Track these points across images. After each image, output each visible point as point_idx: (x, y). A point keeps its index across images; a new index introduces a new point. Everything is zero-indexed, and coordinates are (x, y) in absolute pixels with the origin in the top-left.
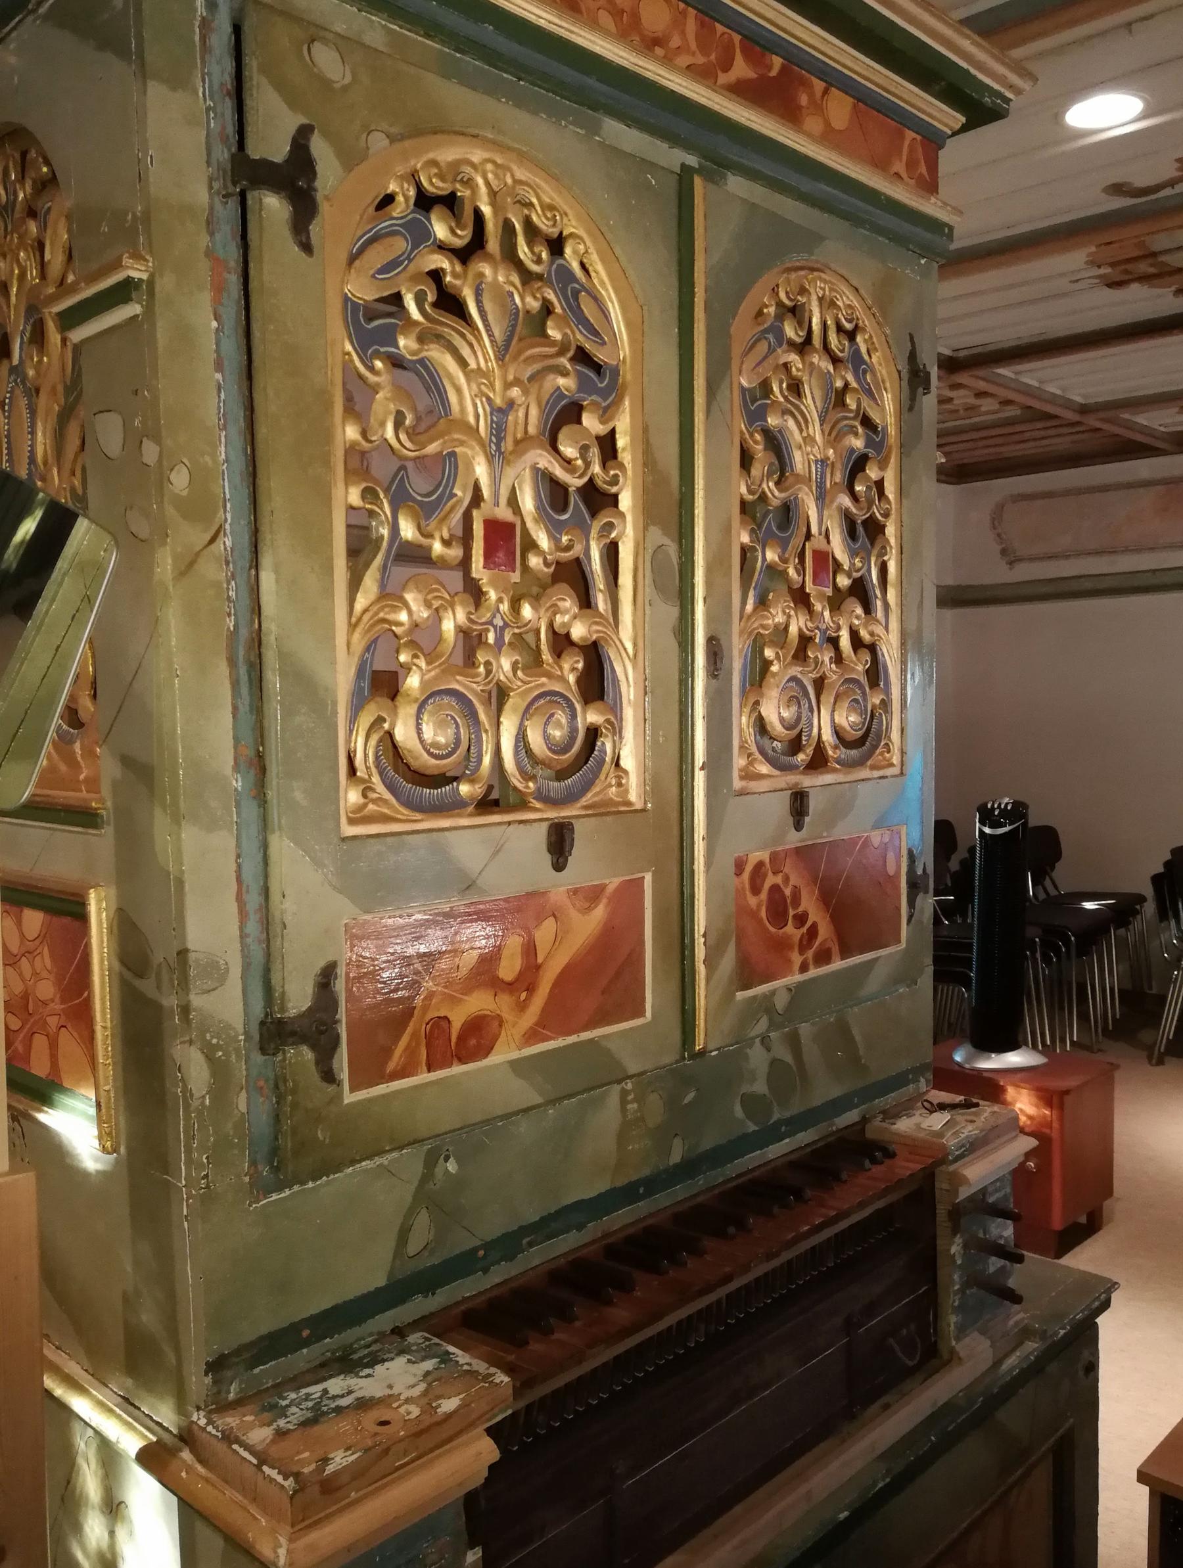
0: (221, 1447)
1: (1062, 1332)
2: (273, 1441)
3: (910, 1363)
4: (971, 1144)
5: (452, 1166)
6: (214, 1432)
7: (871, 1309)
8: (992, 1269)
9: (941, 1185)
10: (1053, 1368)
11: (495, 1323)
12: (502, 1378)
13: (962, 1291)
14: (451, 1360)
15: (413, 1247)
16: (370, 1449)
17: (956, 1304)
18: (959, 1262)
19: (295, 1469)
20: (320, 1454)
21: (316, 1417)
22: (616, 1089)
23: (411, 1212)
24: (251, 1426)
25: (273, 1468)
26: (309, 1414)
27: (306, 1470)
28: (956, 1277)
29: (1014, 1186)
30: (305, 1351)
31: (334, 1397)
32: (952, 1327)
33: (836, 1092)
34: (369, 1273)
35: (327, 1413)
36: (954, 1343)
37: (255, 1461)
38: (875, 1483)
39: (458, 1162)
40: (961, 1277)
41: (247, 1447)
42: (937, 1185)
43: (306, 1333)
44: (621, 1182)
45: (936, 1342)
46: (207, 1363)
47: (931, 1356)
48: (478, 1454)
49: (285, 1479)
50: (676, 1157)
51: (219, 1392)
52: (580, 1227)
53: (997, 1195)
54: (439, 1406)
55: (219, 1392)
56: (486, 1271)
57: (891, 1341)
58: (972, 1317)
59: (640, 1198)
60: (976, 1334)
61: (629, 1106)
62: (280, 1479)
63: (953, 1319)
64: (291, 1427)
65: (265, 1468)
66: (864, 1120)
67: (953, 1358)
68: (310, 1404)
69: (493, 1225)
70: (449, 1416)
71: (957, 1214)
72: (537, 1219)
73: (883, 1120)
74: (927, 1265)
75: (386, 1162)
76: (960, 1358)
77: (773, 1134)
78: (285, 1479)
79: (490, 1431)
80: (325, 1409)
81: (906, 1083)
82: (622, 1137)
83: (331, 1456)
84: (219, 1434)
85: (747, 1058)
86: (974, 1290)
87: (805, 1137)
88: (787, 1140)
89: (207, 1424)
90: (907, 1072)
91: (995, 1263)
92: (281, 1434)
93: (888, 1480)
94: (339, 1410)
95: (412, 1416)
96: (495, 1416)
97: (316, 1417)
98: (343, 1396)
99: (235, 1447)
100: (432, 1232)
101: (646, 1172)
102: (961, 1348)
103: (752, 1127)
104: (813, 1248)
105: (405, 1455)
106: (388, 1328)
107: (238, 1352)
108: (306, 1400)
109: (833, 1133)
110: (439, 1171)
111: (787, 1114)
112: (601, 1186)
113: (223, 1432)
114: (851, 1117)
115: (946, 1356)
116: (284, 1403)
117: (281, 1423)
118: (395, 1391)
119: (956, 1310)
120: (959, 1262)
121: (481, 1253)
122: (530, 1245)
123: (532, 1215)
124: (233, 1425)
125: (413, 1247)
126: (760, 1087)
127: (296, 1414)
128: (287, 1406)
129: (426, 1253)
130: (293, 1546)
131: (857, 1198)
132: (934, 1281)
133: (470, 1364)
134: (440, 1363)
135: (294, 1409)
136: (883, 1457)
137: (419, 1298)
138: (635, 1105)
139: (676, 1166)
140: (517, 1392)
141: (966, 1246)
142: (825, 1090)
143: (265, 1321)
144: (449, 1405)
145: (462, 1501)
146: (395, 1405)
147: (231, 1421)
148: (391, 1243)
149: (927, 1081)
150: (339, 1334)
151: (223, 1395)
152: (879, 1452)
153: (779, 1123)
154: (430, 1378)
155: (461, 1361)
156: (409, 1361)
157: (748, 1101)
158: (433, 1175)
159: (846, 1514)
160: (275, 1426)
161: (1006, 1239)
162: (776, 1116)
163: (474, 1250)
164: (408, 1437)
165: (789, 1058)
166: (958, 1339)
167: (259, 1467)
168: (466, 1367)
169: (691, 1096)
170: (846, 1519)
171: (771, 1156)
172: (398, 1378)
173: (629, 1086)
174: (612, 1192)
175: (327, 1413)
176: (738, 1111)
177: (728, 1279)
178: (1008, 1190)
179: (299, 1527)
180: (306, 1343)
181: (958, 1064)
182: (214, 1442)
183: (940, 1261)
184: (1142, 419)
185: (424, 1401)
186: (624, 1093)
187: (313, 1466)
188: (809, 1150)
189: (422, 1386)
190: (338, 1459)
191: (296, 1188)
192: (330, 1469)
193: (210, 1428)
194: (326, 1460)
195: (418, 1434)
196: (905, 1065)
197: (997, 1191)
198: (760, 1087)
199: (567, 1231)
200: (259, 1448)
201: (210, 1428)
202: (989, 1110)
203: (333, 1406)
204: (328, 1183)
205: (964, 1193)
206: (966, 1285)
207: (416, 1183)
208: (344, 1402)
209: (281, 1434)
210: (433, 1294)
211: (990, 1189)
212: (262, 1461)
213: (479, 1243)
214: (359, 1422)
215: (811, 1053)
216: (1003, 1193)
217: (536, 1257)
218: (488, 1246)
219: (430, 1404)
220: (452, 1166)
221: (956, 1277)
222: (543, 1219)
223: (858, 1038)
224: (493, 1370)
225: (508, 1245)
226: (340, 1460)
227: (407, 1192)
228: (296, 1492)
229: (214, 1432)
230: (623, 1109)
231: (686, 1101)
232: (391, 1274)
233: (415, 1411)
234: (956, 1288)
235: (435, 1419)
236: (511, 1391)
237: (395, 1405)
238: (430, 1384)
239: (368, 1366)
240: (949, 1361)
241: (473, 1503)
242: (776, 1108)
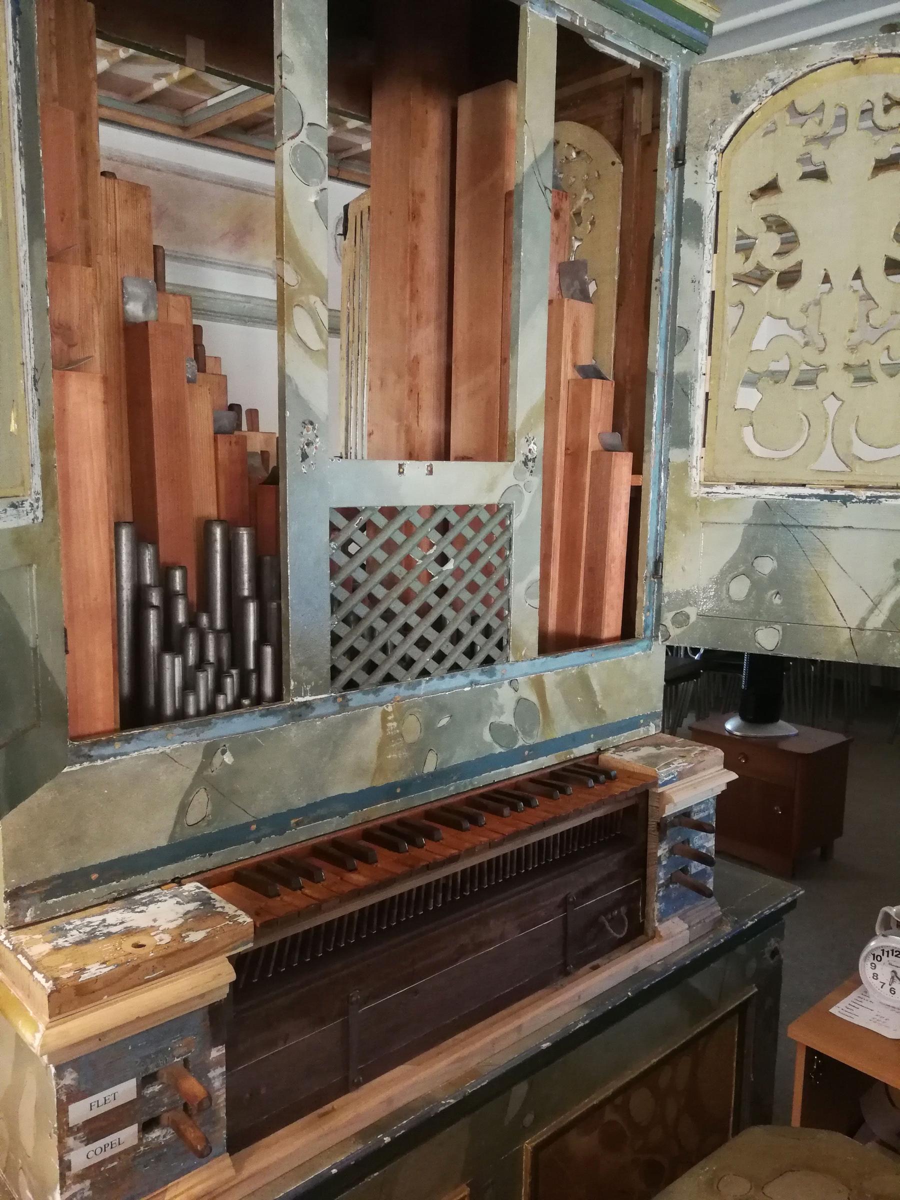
0: (10, 956)
1: (750, 923)
2: (48, 954)
3: (618, 936)
4: (679, 773)
5: (228, 759)
6: (8, 945)
7: (587, 893)
8: (693, 871)
9: (652, 802)
10: (741, 949)
11: (256, 881)
12: (245, 919)
13: (666, 885)
14: (210, 904)
15: (193, 817)
16: (122, 964)
17: (661, 894)
18: (664, 863)
19: (56, 975)
20: (80, 965)
21: (90, 938)
22: (379, 709)
23: (190, 792)
24: (36, 942)
25: (41, 973)
26: (84, 937)
27: (64, 977)
28: (661, 874)
29: (717, 811)
30: (94, 890)
31: (109, 925)
32: (656, 913)
33: (574, 728)
34: (154, 833)
35: (99, 936)
36: (657, 924)
37: (30, 968)
38: (576, 1023)
39: (234, 755)
40: (665, 874)
41: (27, 958)
42: (650, 803)
43: (94, 877)
44: (380, 782)
45: (643, 922)
46: (5, 892)
47: (638, 931)
48: (215, 977)
49: (47, 982)
50: (430, 766)
51: (16, 915)
52: (343, 815)
53: (702, 815)
54: (188, 936)
55: (16, 915)
56: (258, 841)
57: (603, 918)
58: (673, 907)
59: (397, 796)
60: (677, 919)
61: (389, 725)
62: (43, 981)
63: (657, 906)
64: (67, 944)
65: (35, 973)
66: (599, 751)
67: (655, 936)
68: (88, 929)
69: (265, 804)
70: (194, 945)
71: (663, 826)
72: (305, 805)
73: (614, 752)
74: (639, 863)
75: (168, 751)
76: (661, 937)
77: (518, 756)
78: (47, 982)
79: (230, 959)
80: (98, 933)
81: (638, 726)
82: (382, 749)
83: (87, 967)
84: (11, 947)
85: (496, 695)
86: (678, 885)
87: (547, 761)
88: (530, 762)
89: (5, 939)
90: (639, 717)
91: (696, 867)
92: (57, 949)
93: (587, 1022)
94: (109, 934)
95: (163, 943)
96: (238, 947)
97: (90, 938)
98: (116, 925)
99: (20, 956)
100: (210, 808)
101: (402, 776)
102: (663, 928)
103: (498, 750)
104: (540, 842)
105: (154, 972)
106: (169, 878)
107: (30, 887)
108: (87, 926)
109: (571, 760)
110: (216, 761)
111: (531, 742)
112: (363, 784)
113: (14, 945)
114: (588, 749)
115: (650, 933)
116: (68, 927)
117: (61, 942)
118: (157, 924)
119: (659, 899)
120: (664, 863)
121: (254, 827)
122: (298, 824)
123: (299, 801)
124: (24, 940)
125: (193, 817)
126: (507, 719)
127: (75, 936)
128: (70, 930)
129: (204, 824)
130: (48, 1032)
131: (581, 811)
132: (644, 877)
133: (223, 907)
134: (201, 905)
135: (75, 932)
136: (586, 1004)
137: (197, 858)
138: (395, 724)
139: (431, 774)
140: (259, 931)
141: (671, 851)
142: (565, 724)
143: (59, 864)
144: (196, 936)
145: (206, 1010)
146: (152, 934)
147: (22, 937)
148: (172, 812)
149: (657, 726)
150: (123, 878)
151: (20, 918)
152: (582, 1002)
153: (523, 748)
154: (188, 916)
155: (218, 904)
156: (178, 903)
157: (495, 729)
158: (211, 763)
159: (548, 1044)
160: (54, 943)
161: (708, 849)
162: (520, 743)
163: (248, 824)
164: (157, 958)
165: (533, 698)
166: (660, 921)
167: (31, 972)
168: (220, 910)
169: (444, 721)
170: (548, 1048)
171: (515, 774)
172: (163, 914)
173: (390, 709)
174: (372, 789)
175: (99, 936)
176: (487, 737)
177: (453, 859)
178: (712, 811)
179: (55, 1018)
180: (96, 884)
181: (730, 732)
182: (7, 953)
183: (650, 861)
184: (592, 41)
185: (178, 931)
186: (385, 715)
187: (71, 974)
188: (549, 770)
189: (181, 921)
190: (93, 970)
191: (86, 764)
192: (85, 977)
193: (6, 943)
194: (82, 970)
195: (165, 957)
196: (638, 711)
197: (701, 811)
198: (507, 719)
199: (331, 815)
200: (35, 958)
201: (6, 943)
202: (700, 749)
203: (105, 931)
204: (114, 763)
205: (670, 810)
206: (670, 881)
207: (195, 770)
208: (113, 930)
209: (57, 949)
210: (210, 855)
211: (695, 810)
212: (35, 968)
213: (252, 819)
214: (120, 944)
215: (554, 697)
216: (706, 813)
217: (301, 835)
218: (260, 822)
219: (180, 935)
220: (228, 759)
221: (661, 874)
222: (308, 805)
223: (596, 687)
224: (239, 912)
225: (278, 823)
226: (94, 970)
227: (187, 777)
228: (52, 992)
229: (8, 945)
230: (384, 727)
231: (439, 726)
232: (172, 837)
233: (167, 938)
234: (661, 882)
235: (181, 947)
236: (252, 930)
237: (152, 934)
238: (186, 920)
239: (144, 904)
240: (653, 937)
241: (214, 1011)
242: (520, 736)
